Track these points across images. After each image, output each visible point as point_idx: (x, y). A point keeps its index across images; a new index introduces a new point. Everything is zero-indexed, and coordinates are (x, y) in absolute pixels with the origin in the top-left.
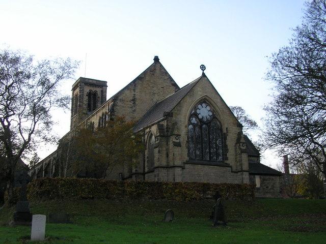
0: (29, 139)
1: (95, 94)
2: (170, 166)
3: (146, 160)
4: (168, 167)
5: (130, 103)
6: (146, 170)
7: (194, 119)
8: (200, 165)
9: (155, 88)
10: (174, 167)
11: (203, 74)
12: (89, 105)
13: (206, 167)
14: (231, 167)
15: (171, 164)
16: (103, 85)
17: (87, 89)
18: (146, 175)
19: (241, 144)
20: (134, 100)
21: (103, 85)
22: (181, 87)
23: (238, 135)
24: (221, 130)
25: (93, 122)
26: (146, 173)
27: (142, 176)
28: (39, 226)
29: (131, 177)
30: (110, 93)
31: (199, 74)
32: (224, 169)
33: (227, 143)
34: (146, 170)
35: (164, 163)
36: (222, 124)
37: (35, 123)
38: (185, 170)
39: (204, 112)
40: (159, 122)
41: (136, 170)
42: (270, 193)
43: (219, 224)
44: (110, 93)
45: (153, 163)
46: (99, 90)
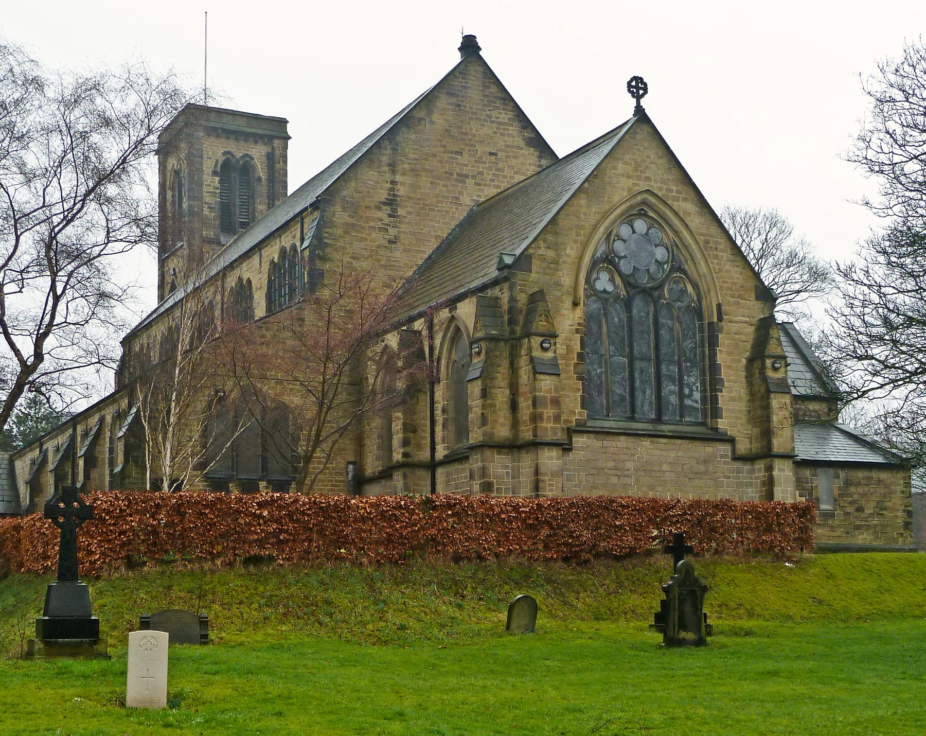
0: (39, 356)
1: (246, 168)
2: (520, 442)
3: (440, 419)
4: (513, 447)
5: (380, 214)
6: (441, 452)
7: (604, 276)
8: (623, 438)
9: (464, 159)
10: (535, 445)
11: (640, 112)
12: (225, 210)
13: (646, 443)
14: (732, 441)
15: (526, 434)
16: (274, 131)
17: (214, 151)
18: (440, 472)
19: (768, 362)
20: (392, 202)
21: (274, 131)
22: (561, 156)
23: (758, 329)
24: (698, 312)
25: (249, 281)
26: (442, 463)
27: (426, 475)
28: (147, 662)
29: (390, 476)
30: (304, 164)
31: (625, 110)
32: (709, 449)
33: (720, 359)
34: (441, 452)
35: (503, 432)
36: (703, 288)
37: (57, 299)
38: (571, 455)
39: (640, 249)
40: (483, 288)
41: (405, 455)
42: (868, 527)
43: (680, 643)
44: (304, 164)
45: (462, 431)
46: (258, 152)
